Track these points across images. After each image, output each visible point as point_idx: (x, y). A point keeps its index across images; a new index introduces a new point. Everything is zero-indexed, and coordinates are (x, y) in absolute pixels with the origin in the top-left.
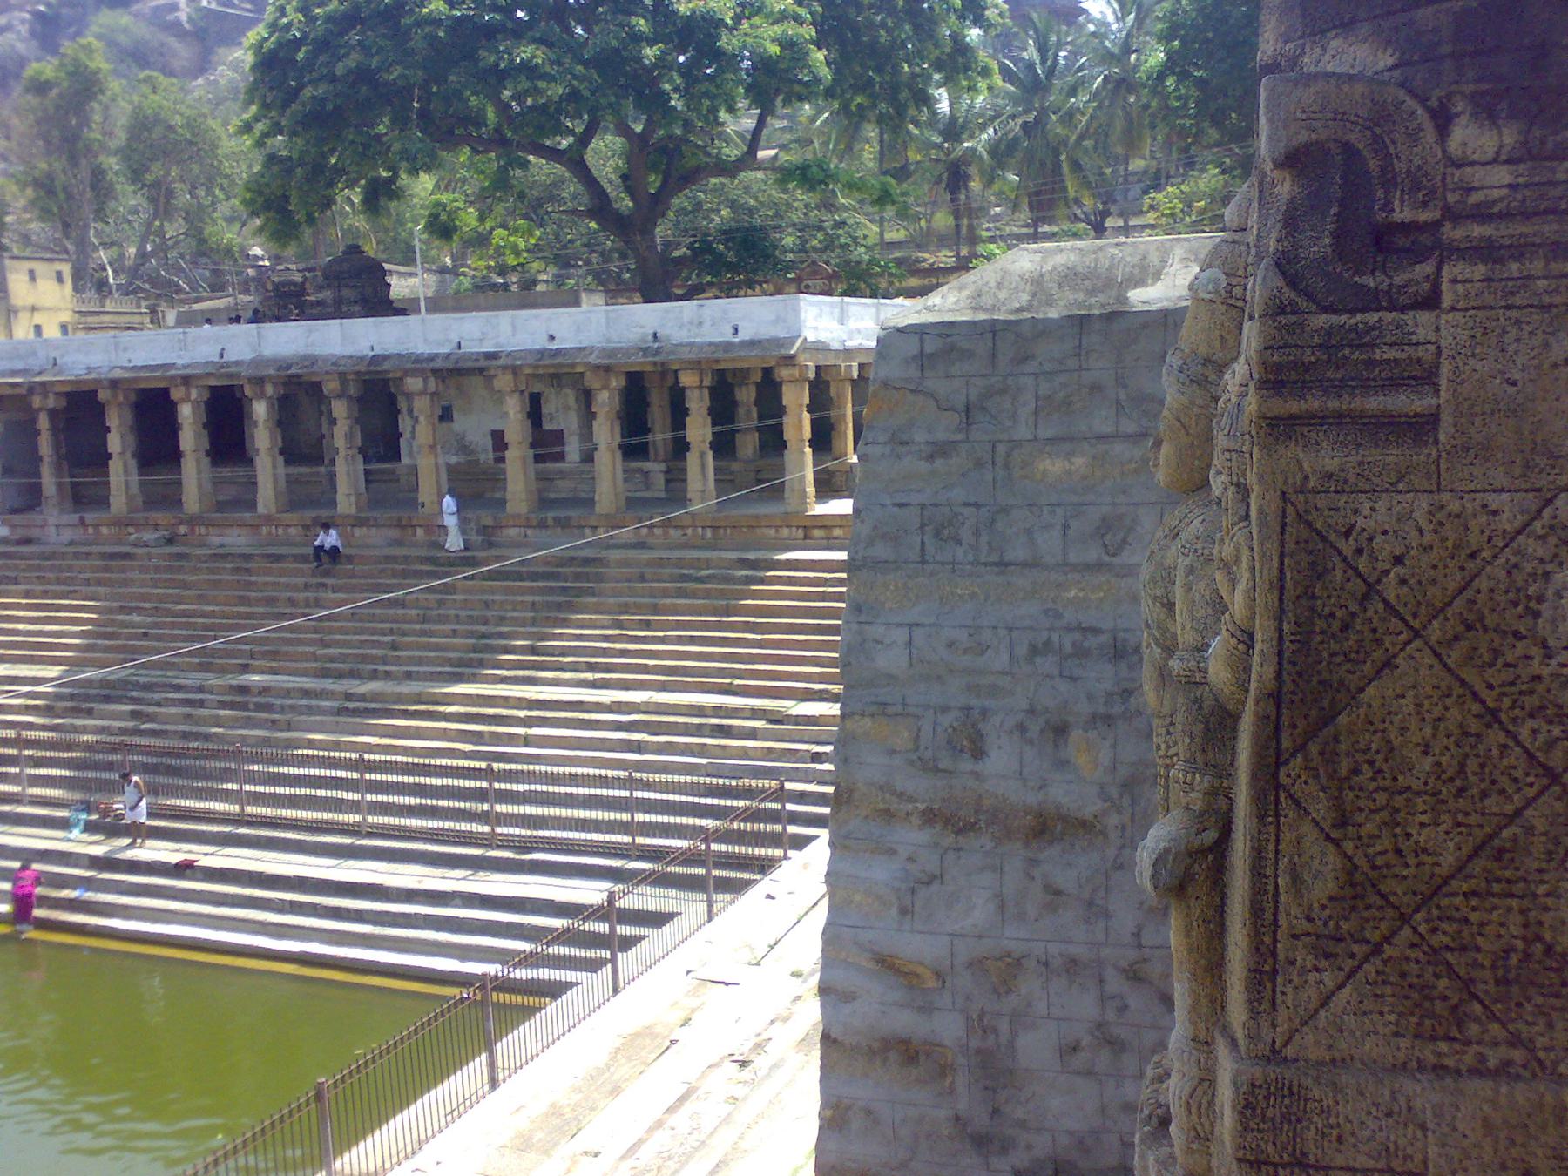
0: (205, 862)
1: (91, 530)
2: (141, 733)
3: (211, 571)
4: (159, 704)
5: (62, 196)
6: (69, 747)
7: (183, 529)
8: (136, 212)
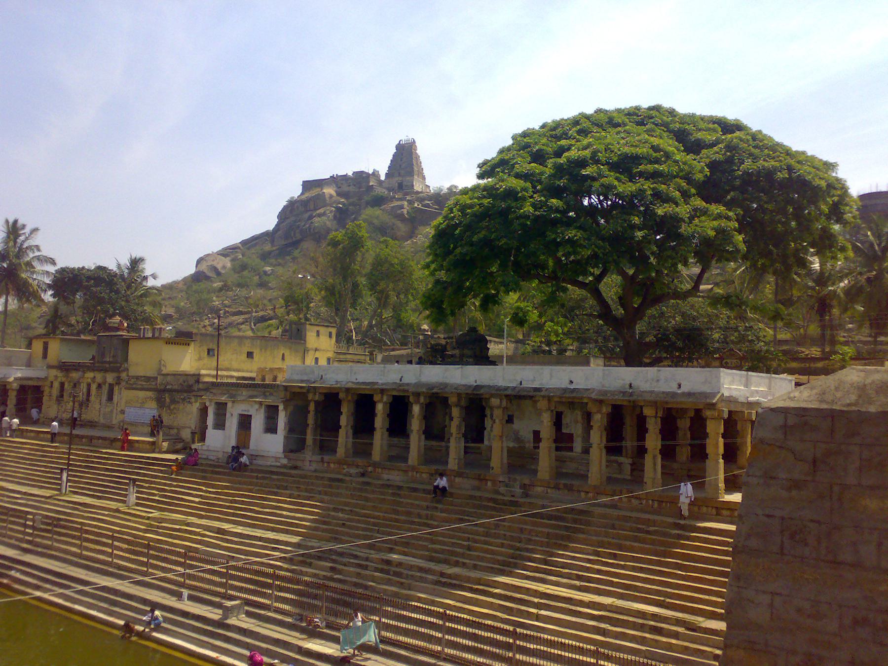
1: (326, 465)
4: (345, 565)
5: (337, 296)
7: (370, 469)
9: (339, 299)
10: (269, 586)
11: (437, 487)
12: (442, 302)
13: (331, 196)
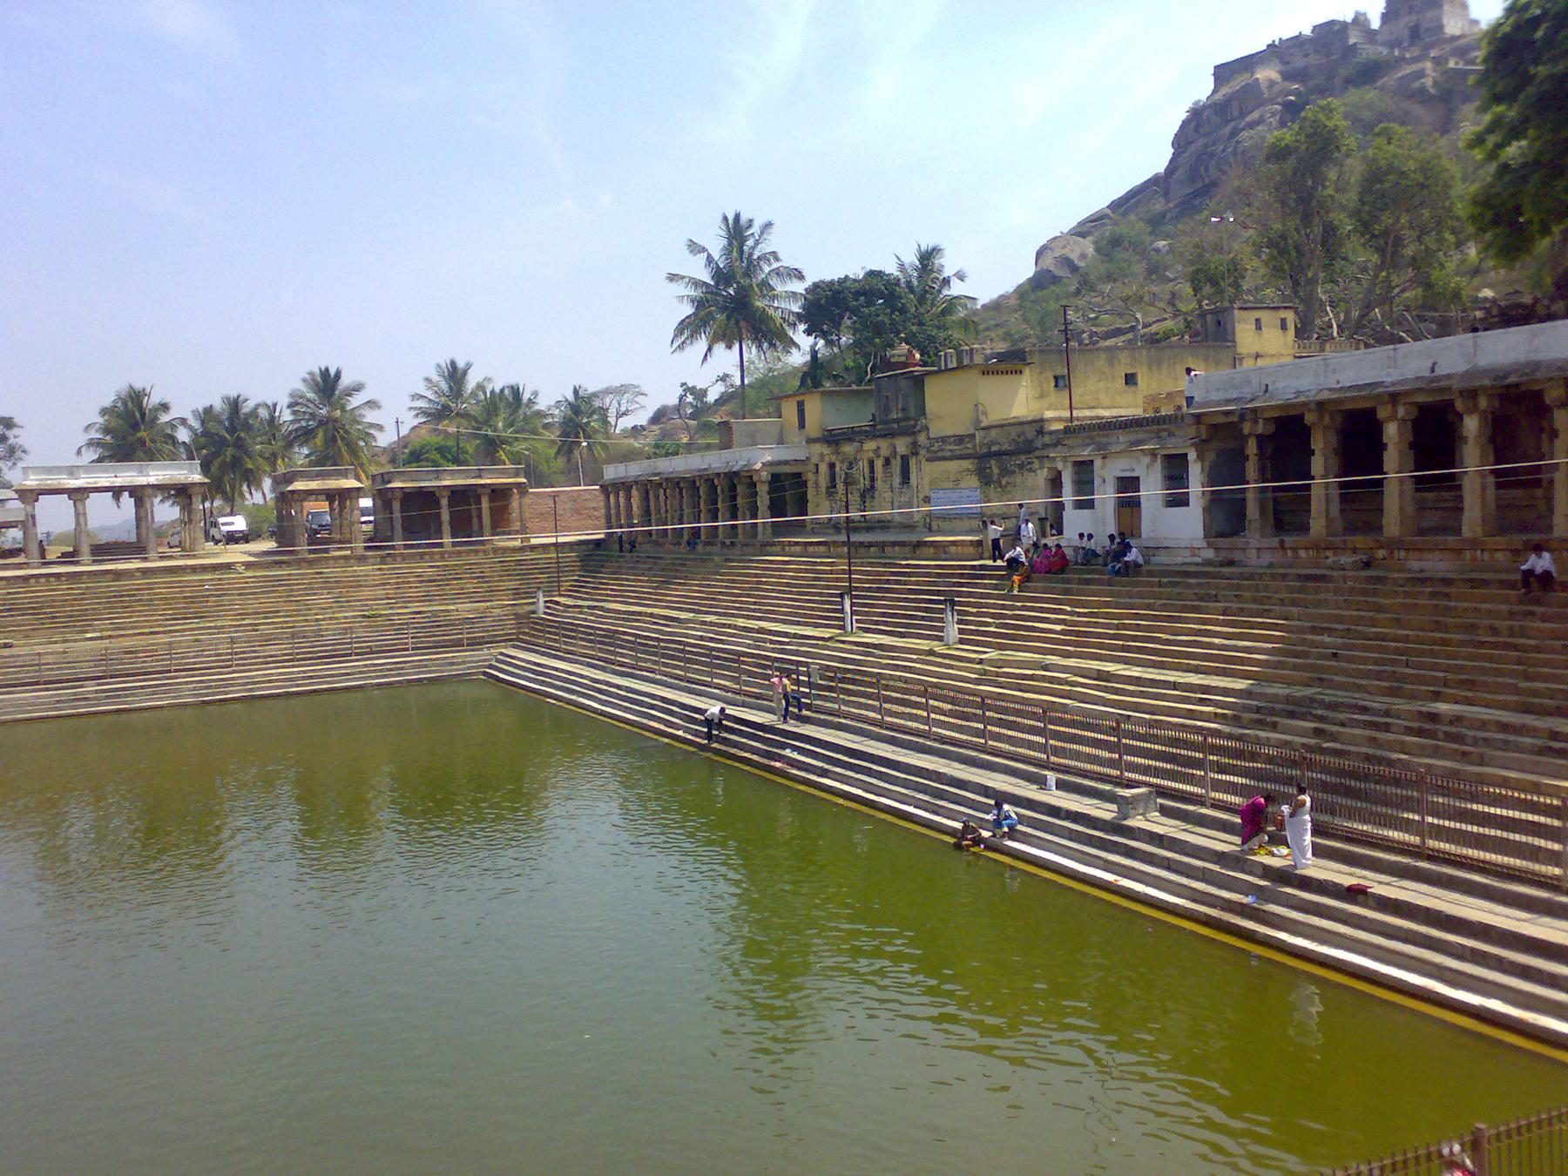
0: (1378, 890)
1: (1289, 553)
2: (1322, 751)
3: (1406, 594)
4: (1343, 725)
5: (1294, 254)
6: (1253, 757)
7: (1381, 553)
8: (1364, 270)
9: (1298, 265)
10: (1199, 764)
11: (1529, 573)
12: (1518, 210)
13: (1272, 83)
